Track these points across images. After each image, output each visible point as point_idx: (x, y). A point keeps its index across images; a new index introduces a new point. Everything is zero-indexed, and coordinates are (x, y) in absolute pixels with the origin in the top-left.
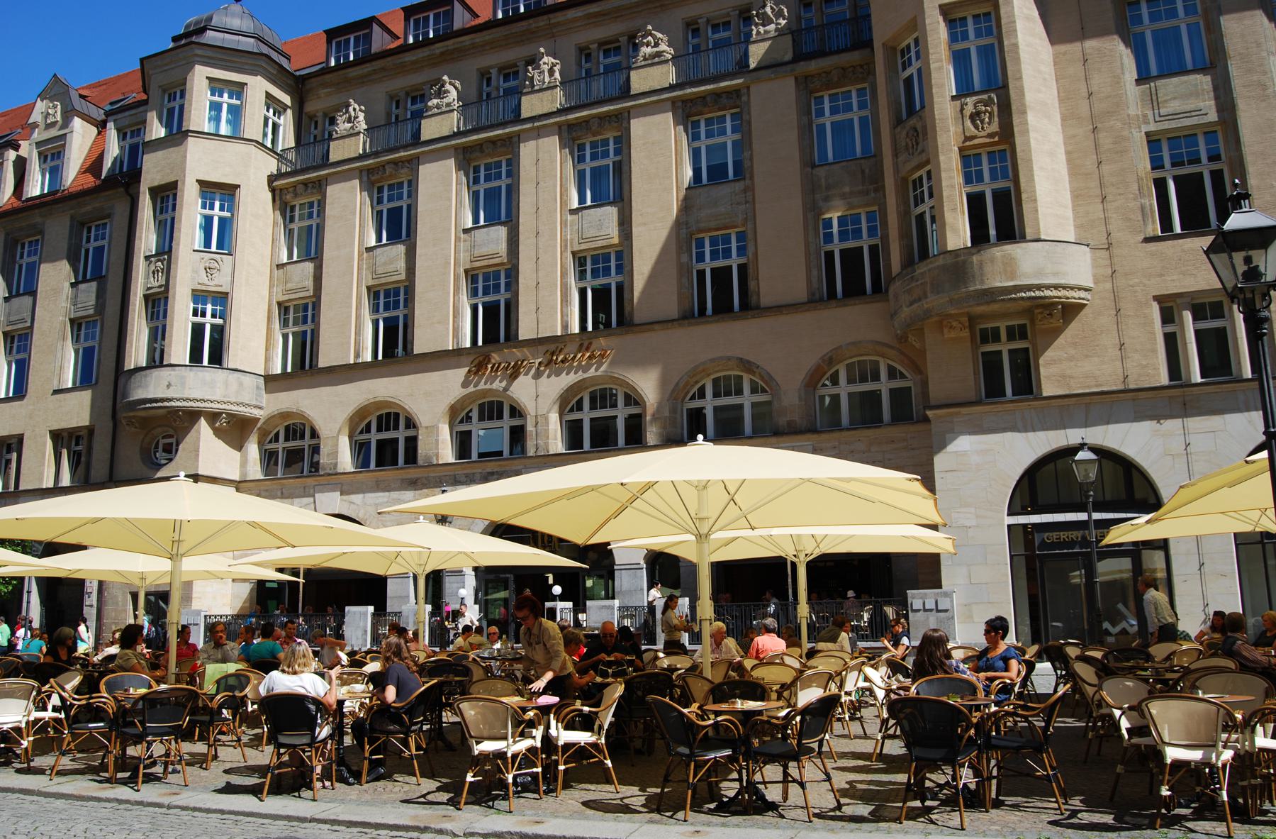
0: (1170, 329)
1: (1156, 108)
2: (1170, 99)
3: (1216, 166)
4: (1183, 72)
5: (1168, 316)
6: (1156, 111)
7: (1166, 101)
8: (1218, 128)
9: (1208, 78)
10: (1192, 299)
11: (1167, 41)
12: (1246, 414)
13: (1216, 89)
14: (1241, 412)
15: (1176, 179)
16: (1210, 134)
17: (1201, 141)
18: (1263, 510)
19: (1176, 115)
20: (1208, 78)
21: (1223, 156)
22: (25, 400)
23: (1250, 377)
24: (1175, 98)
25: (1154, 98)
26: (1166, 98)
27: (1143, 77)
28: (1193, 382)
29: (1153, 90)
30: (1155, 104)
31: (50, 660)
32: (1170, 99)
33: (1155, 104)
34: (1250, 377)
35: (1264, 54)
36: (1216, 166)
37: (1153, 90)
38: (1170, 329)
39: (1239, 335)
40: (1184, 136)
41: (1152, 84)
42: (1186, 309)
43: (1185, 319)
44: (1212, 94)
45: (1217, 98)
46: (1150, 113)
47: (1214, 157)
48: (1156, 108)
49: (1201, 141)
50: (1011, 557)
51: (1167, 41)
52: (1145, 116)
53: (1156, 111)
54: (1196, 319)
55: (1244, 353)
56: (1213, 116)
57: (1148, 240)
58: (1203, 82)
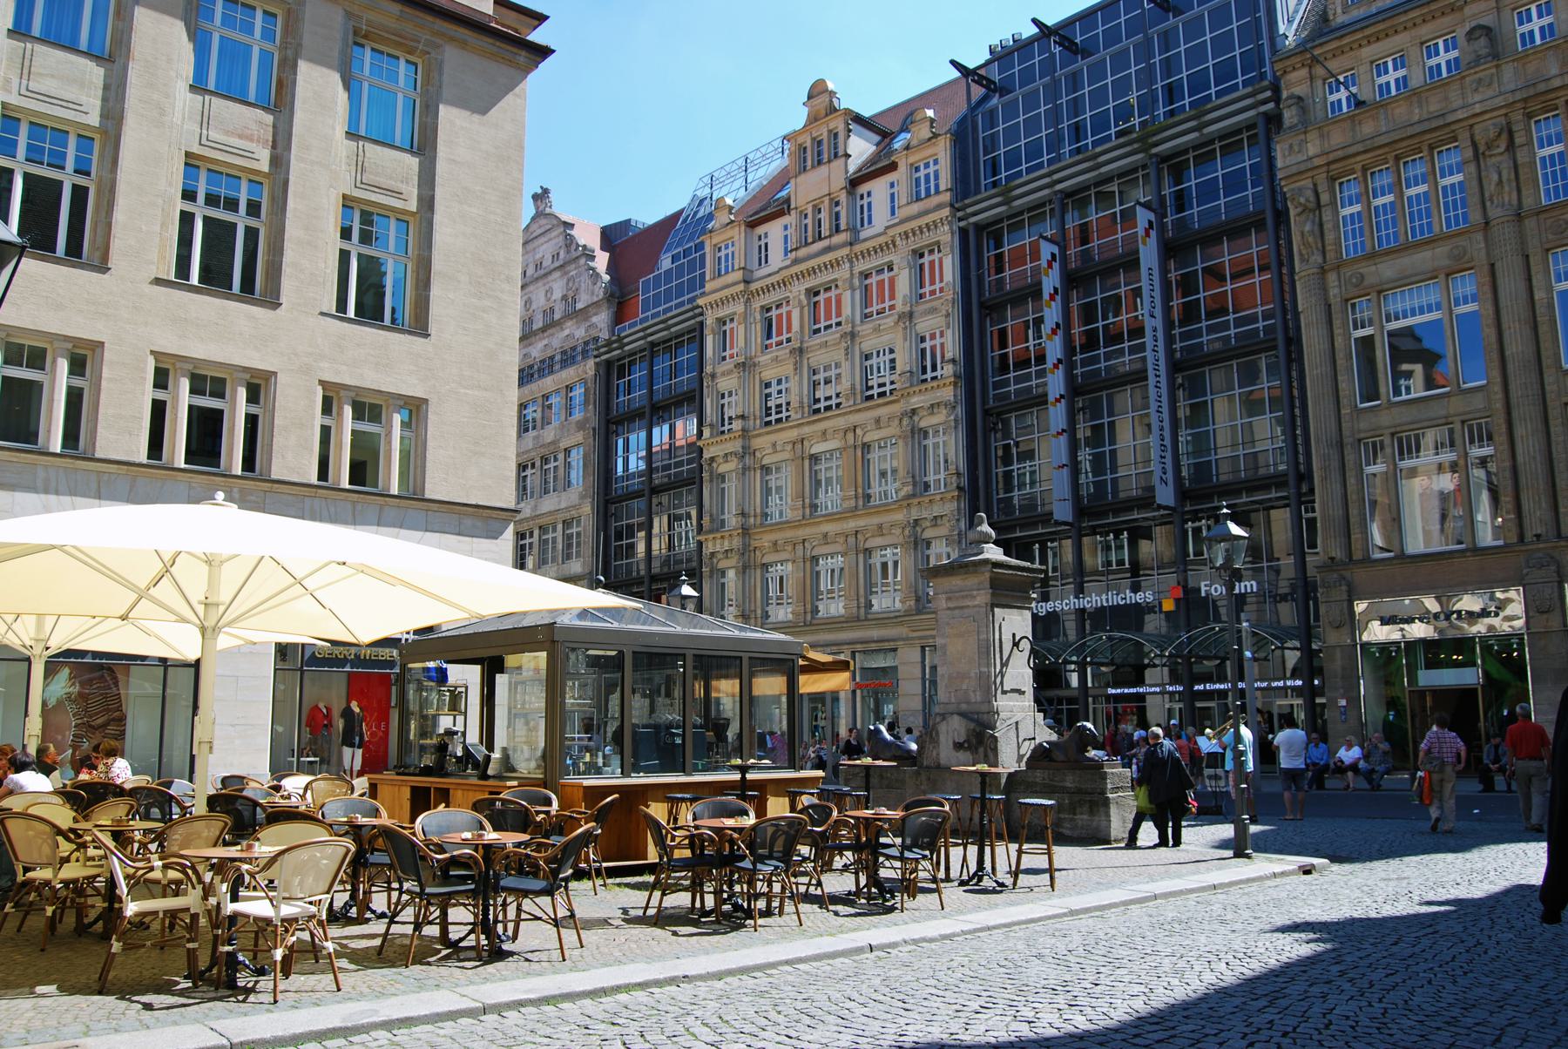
0: (161, 395)
1: (25, 76)
2: (47, 75)
3: (253, 223)
4: (73, 49)
5: (161, 379)
6: (24, 82)
7: (40, 75)
8: (97, 137)
9: (101, 71)
10: (8, 335)
11: (234, 55)
12: (43, 496)
13: (106, 88)
14: (37, 492)
15: (27, 177)
16: (85, 140)
17: (72, 142)
18: (9, 619)
19: (48, 98)
20: (101, 71)
21: (93, 174)
22: (106, 276)
23: (58, 450)
24: (52, 76)
25: (27, 63)
26: (42, 71)
27: (197, 87)
28: (176, 466)
29: (28, 53)
30: (26, 71)
31: (1108, 748)
32: (47, 75)
33: (26, 71)
34: (58, 450)
35: (173, 74)
36: (81, 181)
37: (28, 53)
38: (161, 395)
39: (56, 397)
40: (227, 175)
41: (29, 46)
42: (62, 357)
43: (58, 370)
44: (100, 93)
45: (105, 100)
46: (16, 81)
47: (82, 171)
48: (25, 76)
49: (72, 142)
50: (275, 670)
51: (234, 55)
52: (8, 81)
53: (24, 82)
54: (194, 391)
55: (58, 420)
56: (94, 119)
57: (158, 281)
58: (95, 73)
